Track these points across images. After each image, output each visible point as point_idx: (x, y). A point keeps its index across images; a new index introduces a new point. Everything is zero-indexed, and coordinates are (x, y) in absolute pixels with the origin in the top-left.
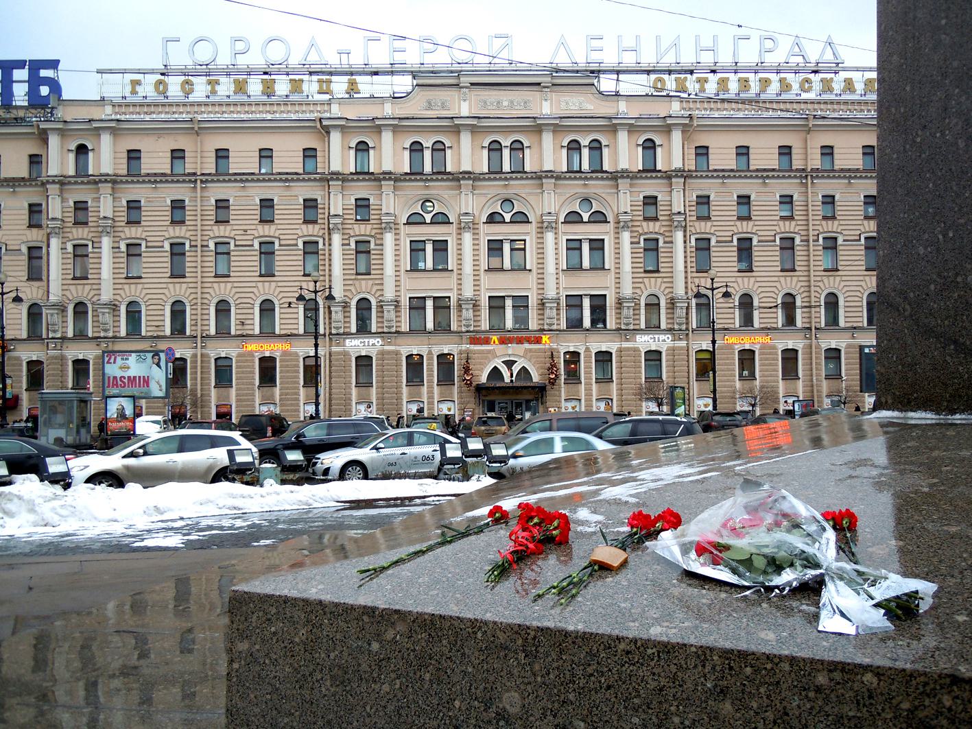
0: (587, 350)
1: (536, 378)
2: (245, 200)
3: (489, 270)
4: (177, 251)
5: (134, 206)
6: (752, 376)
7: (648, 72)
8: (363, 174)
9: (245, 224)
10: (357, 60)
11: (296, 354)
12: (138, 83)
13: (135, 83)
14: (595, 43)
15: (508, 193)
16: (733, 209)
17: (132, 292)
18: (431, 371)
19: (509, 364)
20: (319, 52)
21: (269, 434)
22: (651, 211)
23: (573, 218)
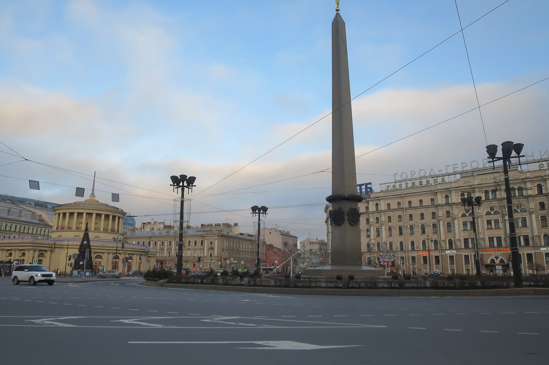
0: (523, 253)
2: (416, 214)
3: (488, 229)
4: (400, 228)
5: (389, 218)
7: (538, 162)
8: (448, 204)
9: (417, 221)
10: (444, 172)
11: (461, 255)
14: (455, 166)
15: (492, 205)
17: (391, 239)
20: (434, 172)
21: (3, 275)
23: (488, 213)
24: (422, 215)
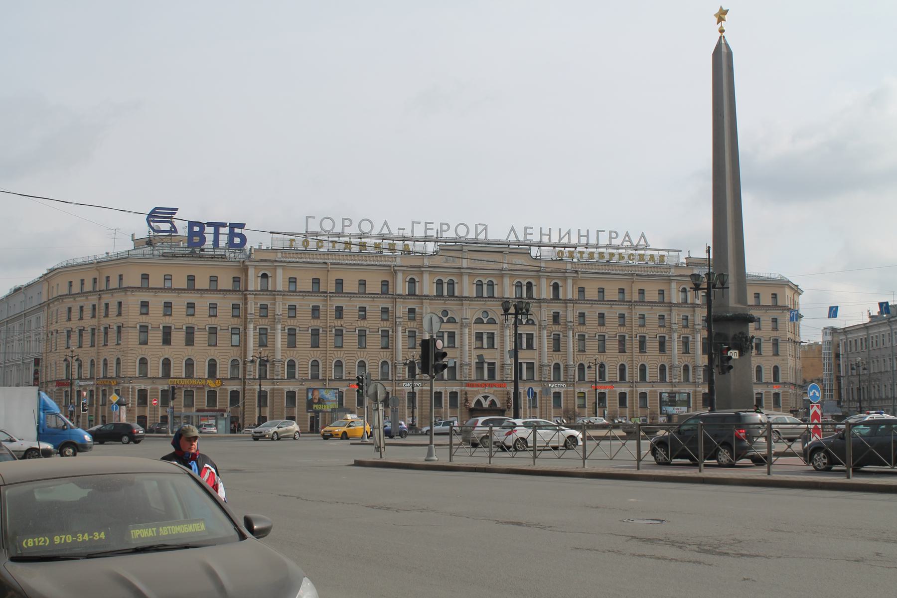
1: (499, 405)
4: (315, 333)
6: (441, 406)
10: (407, 233)
12: (294, 240)
13: (292, 240)
15: (485, 308)
16: (657, 322)
18: (446, 400)
19: (486, 398)
22: (264, 313)
23: (479, 321)
24: (168, 306)
